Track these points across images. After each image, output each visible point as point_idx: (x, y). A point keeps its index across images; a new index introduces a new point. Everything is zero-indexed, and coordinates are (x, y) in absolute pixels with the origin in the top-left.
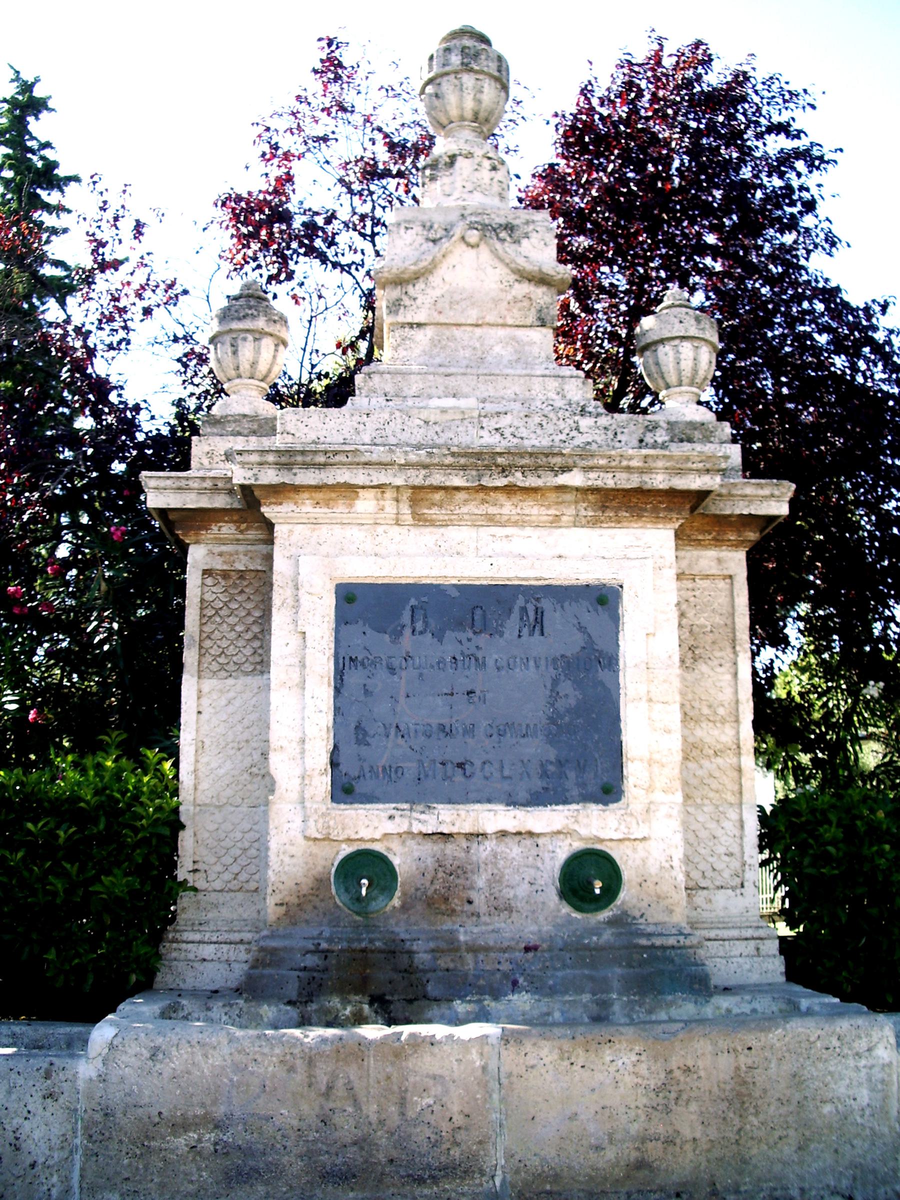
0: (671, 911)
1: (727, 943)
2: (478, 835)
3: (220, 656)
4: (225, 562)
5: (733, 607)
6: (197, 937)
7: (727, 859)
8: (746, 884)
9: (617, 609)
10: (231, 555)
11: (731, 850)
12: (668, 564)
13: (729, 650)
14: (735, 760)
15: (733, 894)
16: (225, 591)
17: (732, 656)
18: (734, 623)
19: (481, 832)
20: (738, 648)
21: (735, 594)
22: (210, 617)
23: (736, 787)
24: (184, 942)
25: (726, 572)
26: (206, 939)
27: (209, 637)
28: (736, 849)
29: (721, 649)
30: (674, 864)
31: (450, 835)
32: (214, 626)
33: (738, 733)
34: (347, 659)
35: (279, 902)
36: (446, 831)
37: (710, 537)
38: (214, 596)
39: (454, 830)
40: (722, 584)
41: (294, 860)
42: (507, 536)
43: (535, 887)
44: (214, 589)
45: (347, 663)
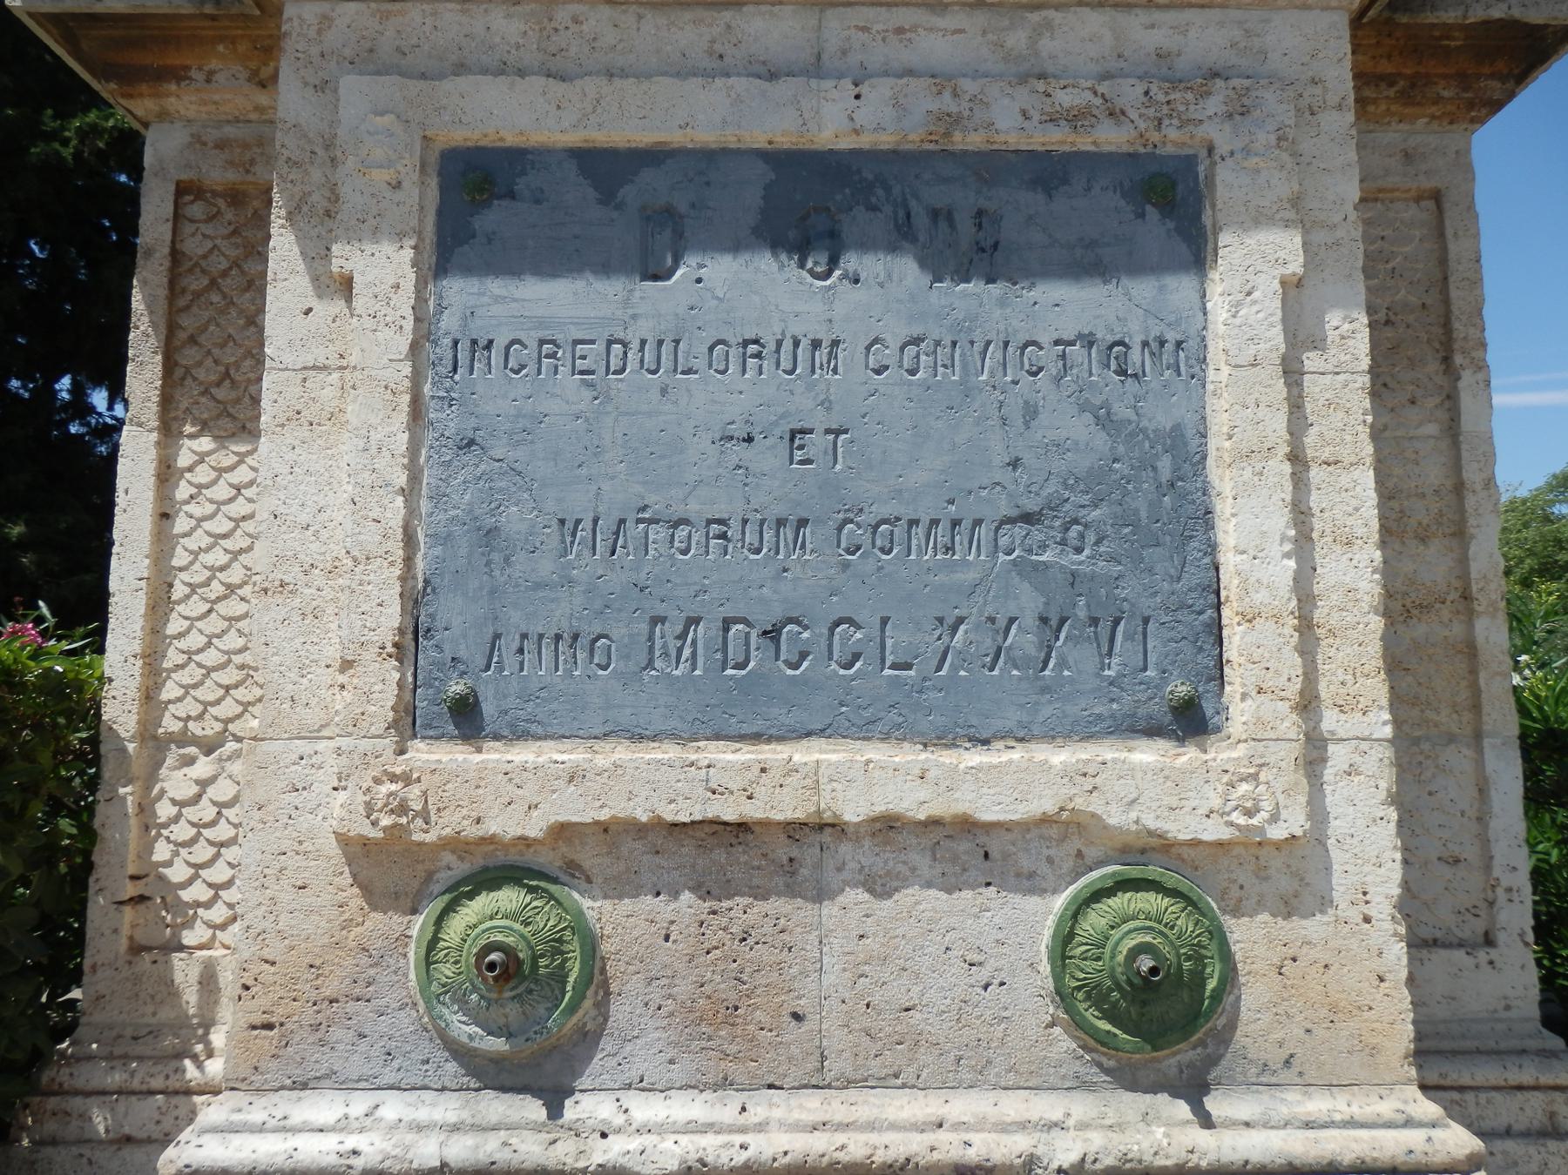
0: (1374, 1051)
1: (1470, 1097)
2: (821, 827)
3: (218, 384)
4: (231, 163)
5: (1443, 261)
6: (116, 1078)
7: (1447, 872)
8: (1501, 937)
9: (1197, 216)
10: (246, 146)
11: (1455, 849)
12: (1333, 99)
13: (1434, 366)
14: (1457, 630)
15: (1469, 961)
16: (235, 232)
17: (1440, 379)
18: (1446, 302)
19: (827, 817)
20: (1458, 359)
21: (1449, 232)
22: (197, 295)
23: (1464, 695)
24: (77, 1093)
25: (1428, 184)
26: (135, 1084)
27: (193, 340)
28: (1470, 852)
29: (1412, 363)
30: (1372, 911)
31: (742, 827)
32: (206, 315)
33: (1464, 561)
34: (463, 347)
35: (258, 1019)
36: (730, 816)
37: (1391, 92)
38: (210, 245)
39: (754, 811)
40: (1410, 212)
41: (307, 898)
42: (900, 31)
43: (982, 975)
44: (208, 229)
45: (463, 356)
